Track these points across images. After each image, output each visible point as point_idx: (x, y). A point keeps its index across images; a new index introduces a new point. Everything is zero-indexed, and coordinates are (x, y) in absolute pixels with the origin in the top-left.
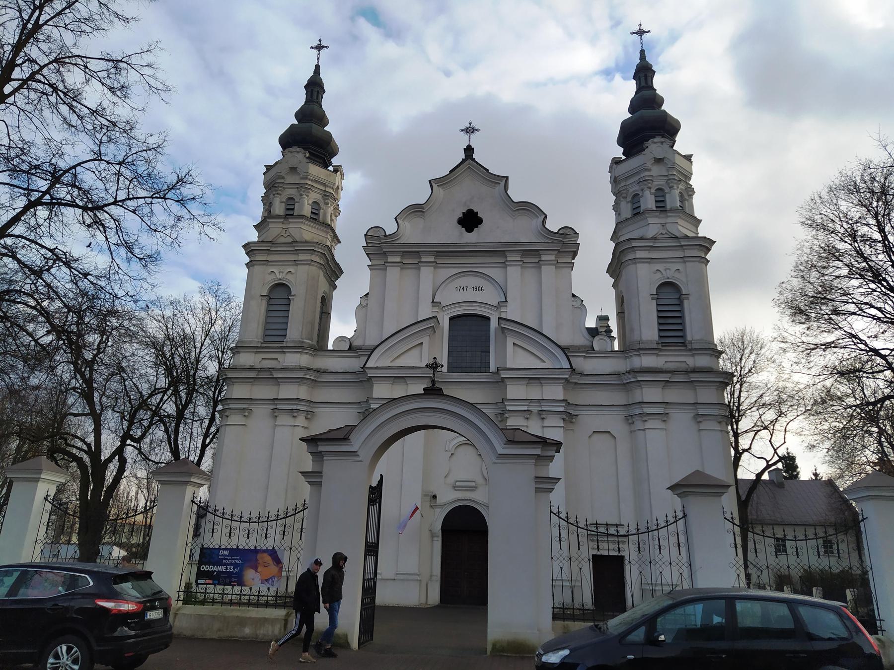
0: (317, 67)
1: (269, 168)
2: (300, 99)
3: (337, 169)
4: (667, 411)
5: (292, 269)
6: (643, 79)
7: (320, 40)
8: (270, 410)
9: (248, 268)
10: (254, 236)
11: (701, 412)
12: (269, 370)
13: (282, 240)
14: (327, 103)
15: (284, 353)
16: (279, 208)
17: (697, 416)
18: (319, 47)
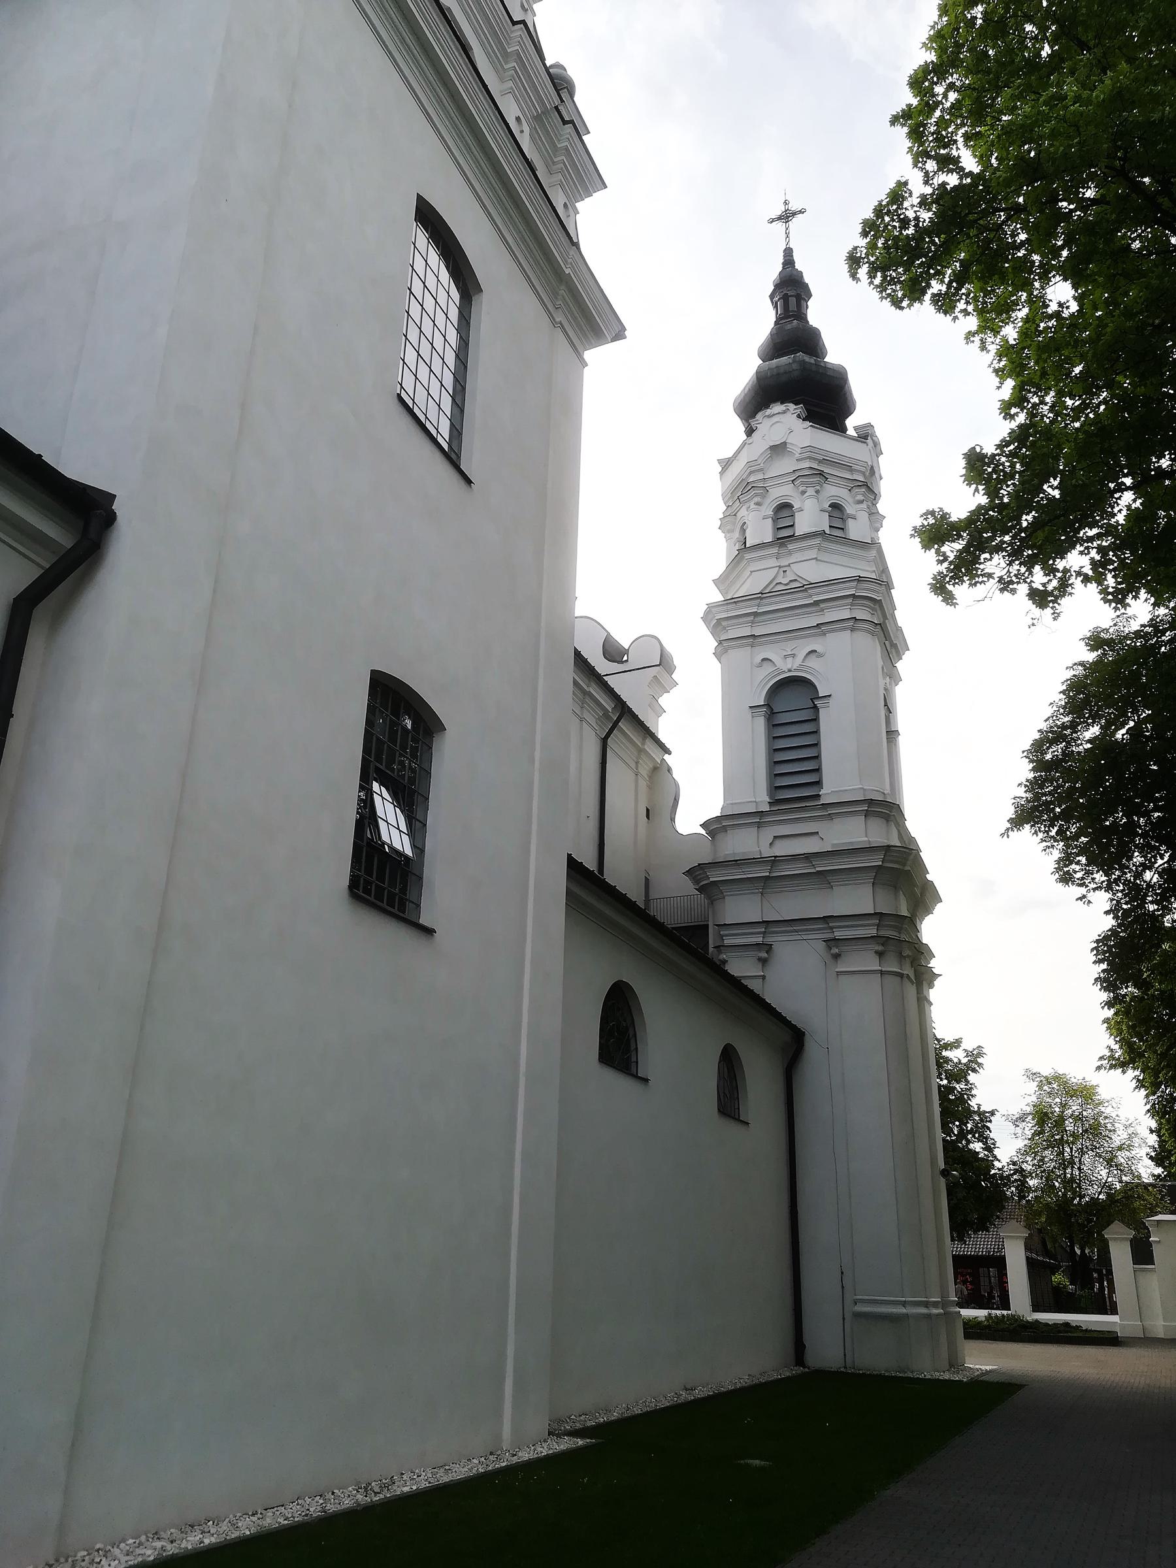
0: (788, 253)
1: (726, 464)
2: (763, 320)
3: (866, 435)
4: (769, 940)
5: (816, 644)
6: (792, 301)
7: (786, 203)
11: (838, 934)
12: (808, 857)
14: (816, 314)
15: (830, 817)
16: (761, 530)
17: (831, 942)
18: (786, 216)
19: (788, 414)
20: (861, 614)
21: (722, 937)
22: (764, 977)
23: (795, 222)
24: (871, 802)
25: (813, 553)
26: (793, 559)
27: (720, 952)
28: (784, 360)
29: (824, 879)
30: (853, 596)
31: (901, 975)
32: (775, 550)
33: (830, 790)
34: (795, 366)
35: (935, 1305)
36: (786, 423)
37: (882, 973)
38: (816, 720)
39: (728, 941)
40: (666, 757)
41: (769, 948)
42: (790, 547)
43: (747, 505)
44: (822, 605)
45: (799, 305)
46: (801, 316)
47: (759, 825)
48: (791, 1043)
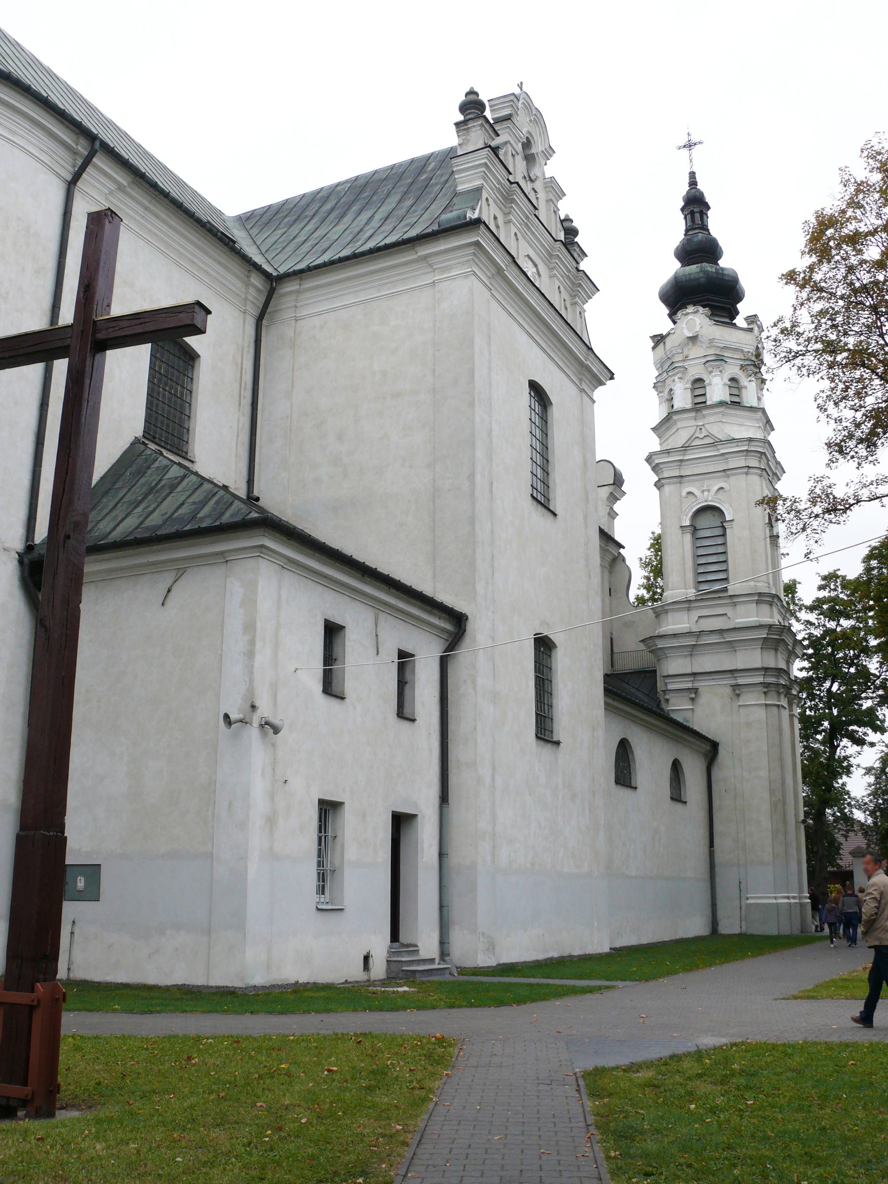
0: (692, 175)
2: (675, 230)
4: (696, 685)
6: (697, 216)
8: (728, 690)
9: (659, 489)
10: (654, 444)
11: (741, 681)
12: (721, 632)
13: (697, 442)
14: (718, 225)
16: (683, 399)
17: (735, 687)
18: (690, 146)
19: (698, 315)
20: (753, 463)
21: (666, 684)
22: (693, 709)
23: (696, 150)
24: (760, 594)
25: (719, 417)
26: (706, 421)
27: (665, 694)
28: (693, 269)
29: (732, 646)
30: (747, 451)
31: (778, 706)
32: (693, 414)
33: (734, 587)
34: (701, 275)
35: (794, 898)
36: (696, 319)
37: (766, 705)
38: (724, 535)
39: (670, 687)
40: (621, 550)
41: (696, 690)
42: (704, 412)
43: (673, 378)
44: (727, 456)
45: (702, 219)
46: (704, 228)
47: (689, 609)
48: (711, 750)
